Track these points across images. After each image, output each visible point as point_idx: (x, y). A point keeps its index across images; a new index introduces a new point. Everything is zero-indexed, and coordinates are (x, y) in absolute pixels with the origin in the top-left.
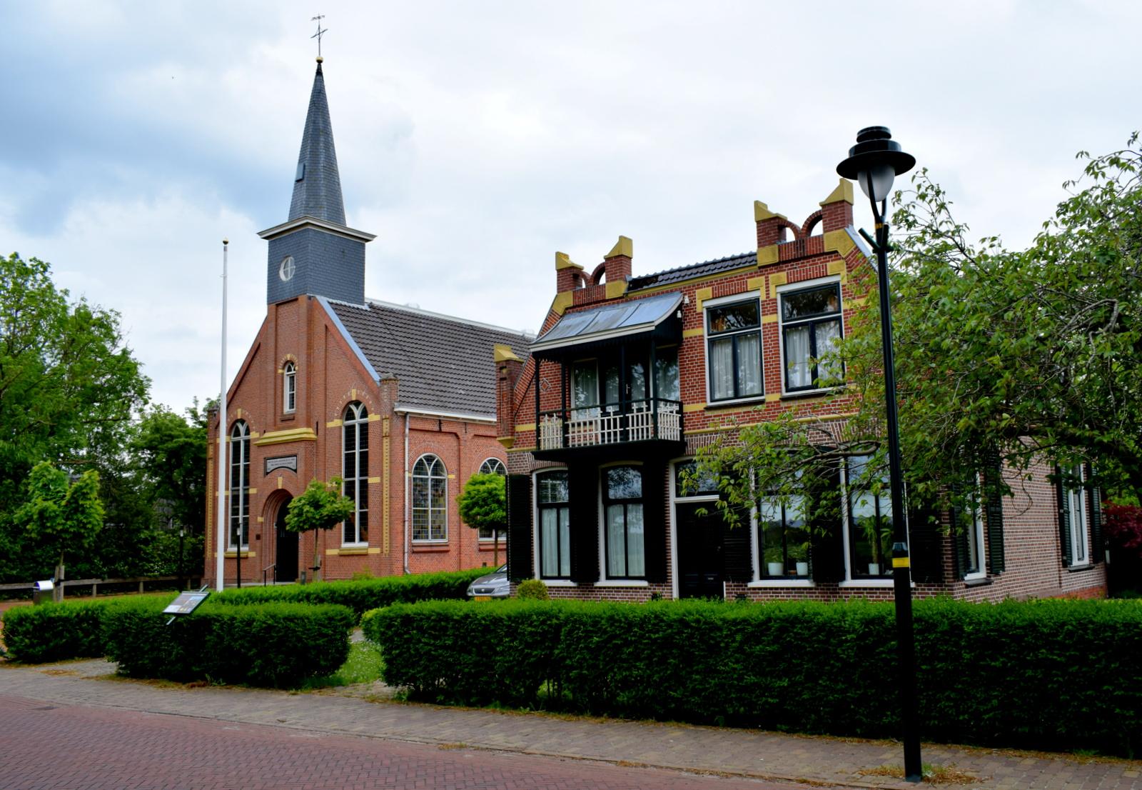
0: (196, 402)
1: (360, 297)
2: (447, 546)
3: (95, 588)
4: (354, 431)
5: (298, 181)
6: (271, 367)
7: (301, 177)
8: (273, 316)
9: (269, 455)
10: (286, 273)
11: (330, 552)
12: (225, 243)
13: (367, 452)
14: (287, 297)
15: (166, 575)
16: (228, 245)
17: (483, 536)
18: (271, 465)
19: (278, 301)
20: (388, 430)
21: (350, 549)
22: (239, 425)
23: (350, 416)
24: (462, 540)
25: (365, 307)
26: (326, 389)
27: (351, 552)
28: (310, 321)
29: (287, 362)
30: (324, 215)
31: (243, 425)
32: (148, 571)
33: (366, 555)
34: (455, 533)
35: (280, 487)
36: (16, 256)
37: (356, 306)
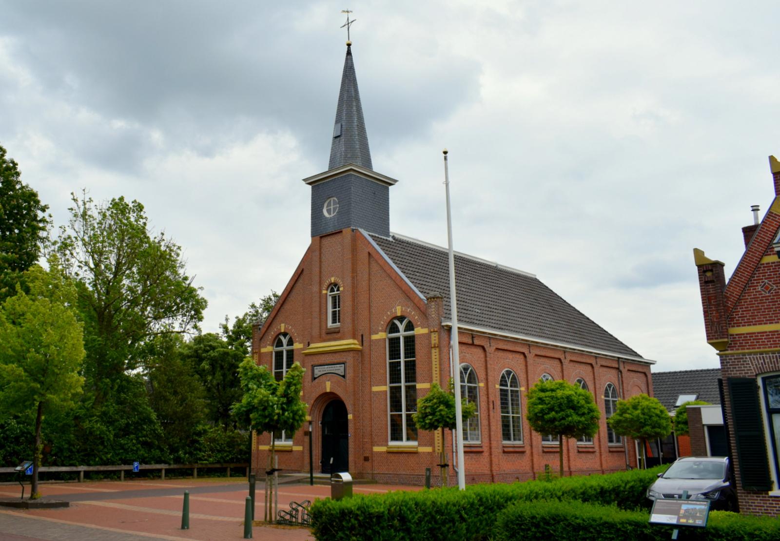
0: (227, 320)
1: (387, 232)
2: (481, 447)
3: (82, 474)
4: (282, 356)
5: (336, 137)
6: (315, 289)
7: (339, 134)
8: (318, 247)
9: (317, 363)
10: (329, 211)
11: (376, 449)
12: (445, 153)
13: (414, 361)
14: (331, 230)
15: (213, 463)
16: (447, 155)
17: (544, 440)
18: (318, 371)
19: (321, 232)
20: (437, 341)
21: (398, 447)
22: (282, 338)
23: (280, 344)
24: (492, 442)
25: (391, 239)
26: (370, 307)
27: (401, 450)
28: (354, 250)
29: (331, 284)
30: (359, 164)
31: (401, 322)
32: (200, 459)
33: (416, 453)
34: (486, 436)
35: (328, 390)
36: (121, 199)
37: (385, 238)
